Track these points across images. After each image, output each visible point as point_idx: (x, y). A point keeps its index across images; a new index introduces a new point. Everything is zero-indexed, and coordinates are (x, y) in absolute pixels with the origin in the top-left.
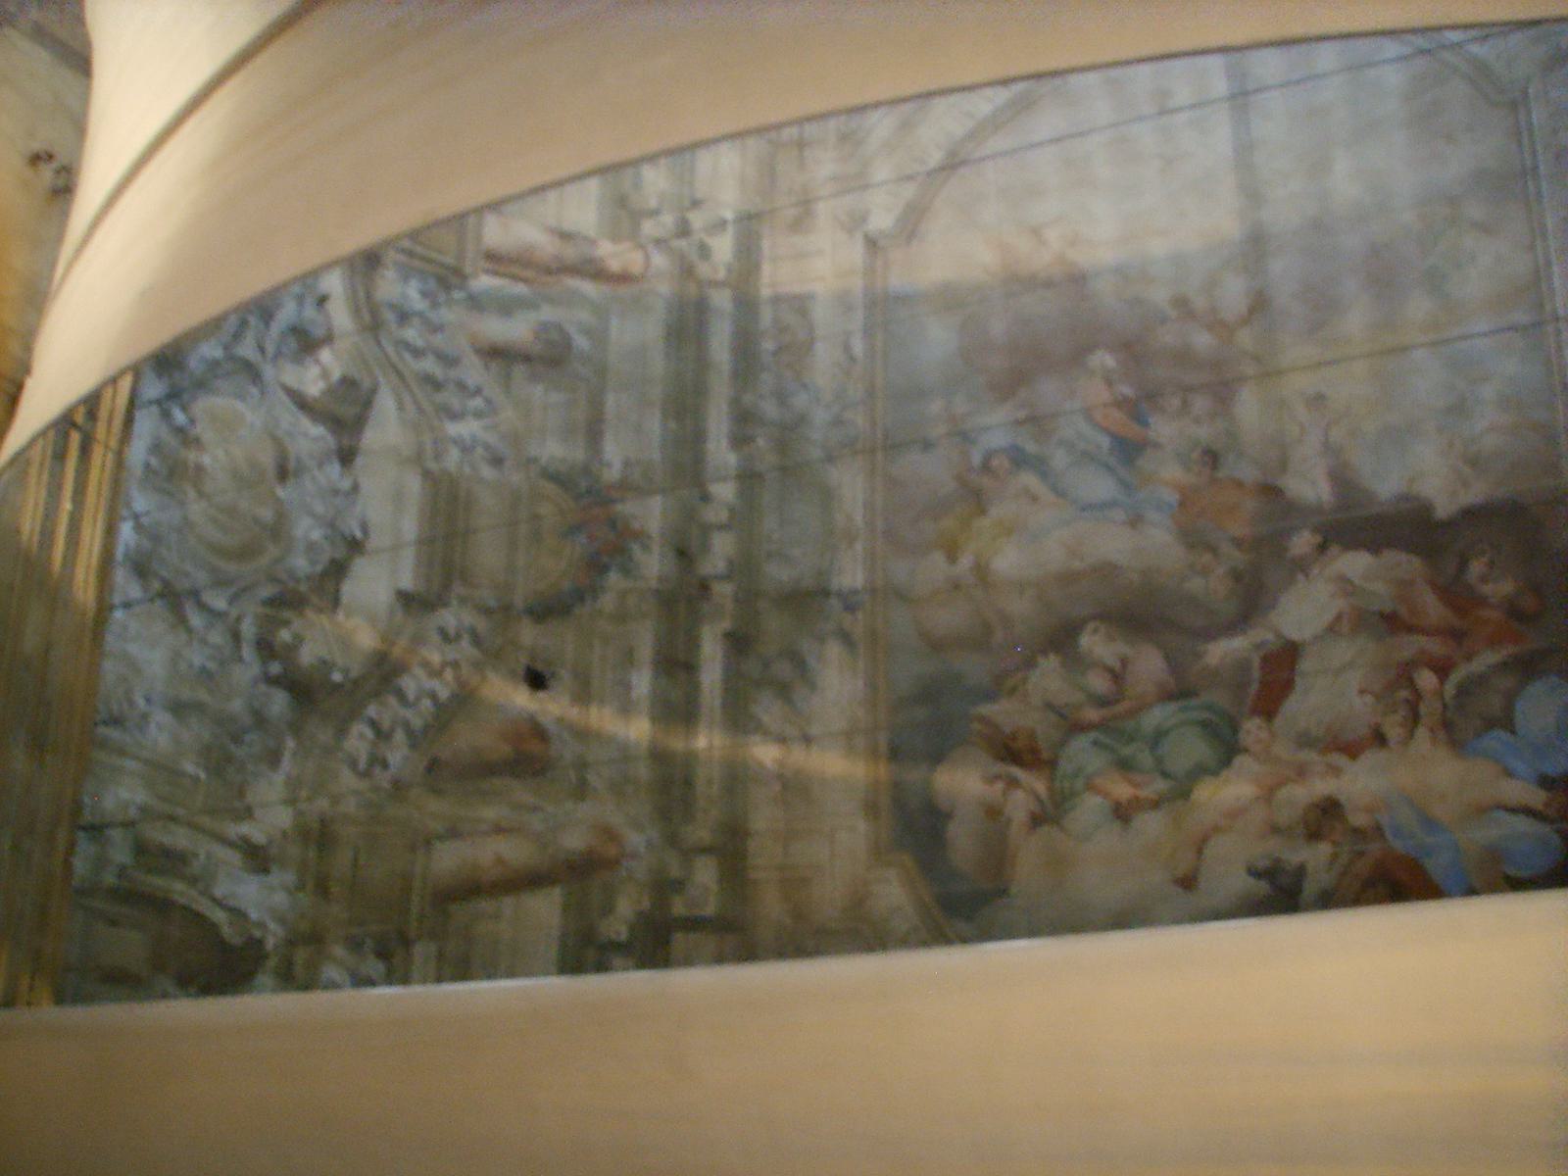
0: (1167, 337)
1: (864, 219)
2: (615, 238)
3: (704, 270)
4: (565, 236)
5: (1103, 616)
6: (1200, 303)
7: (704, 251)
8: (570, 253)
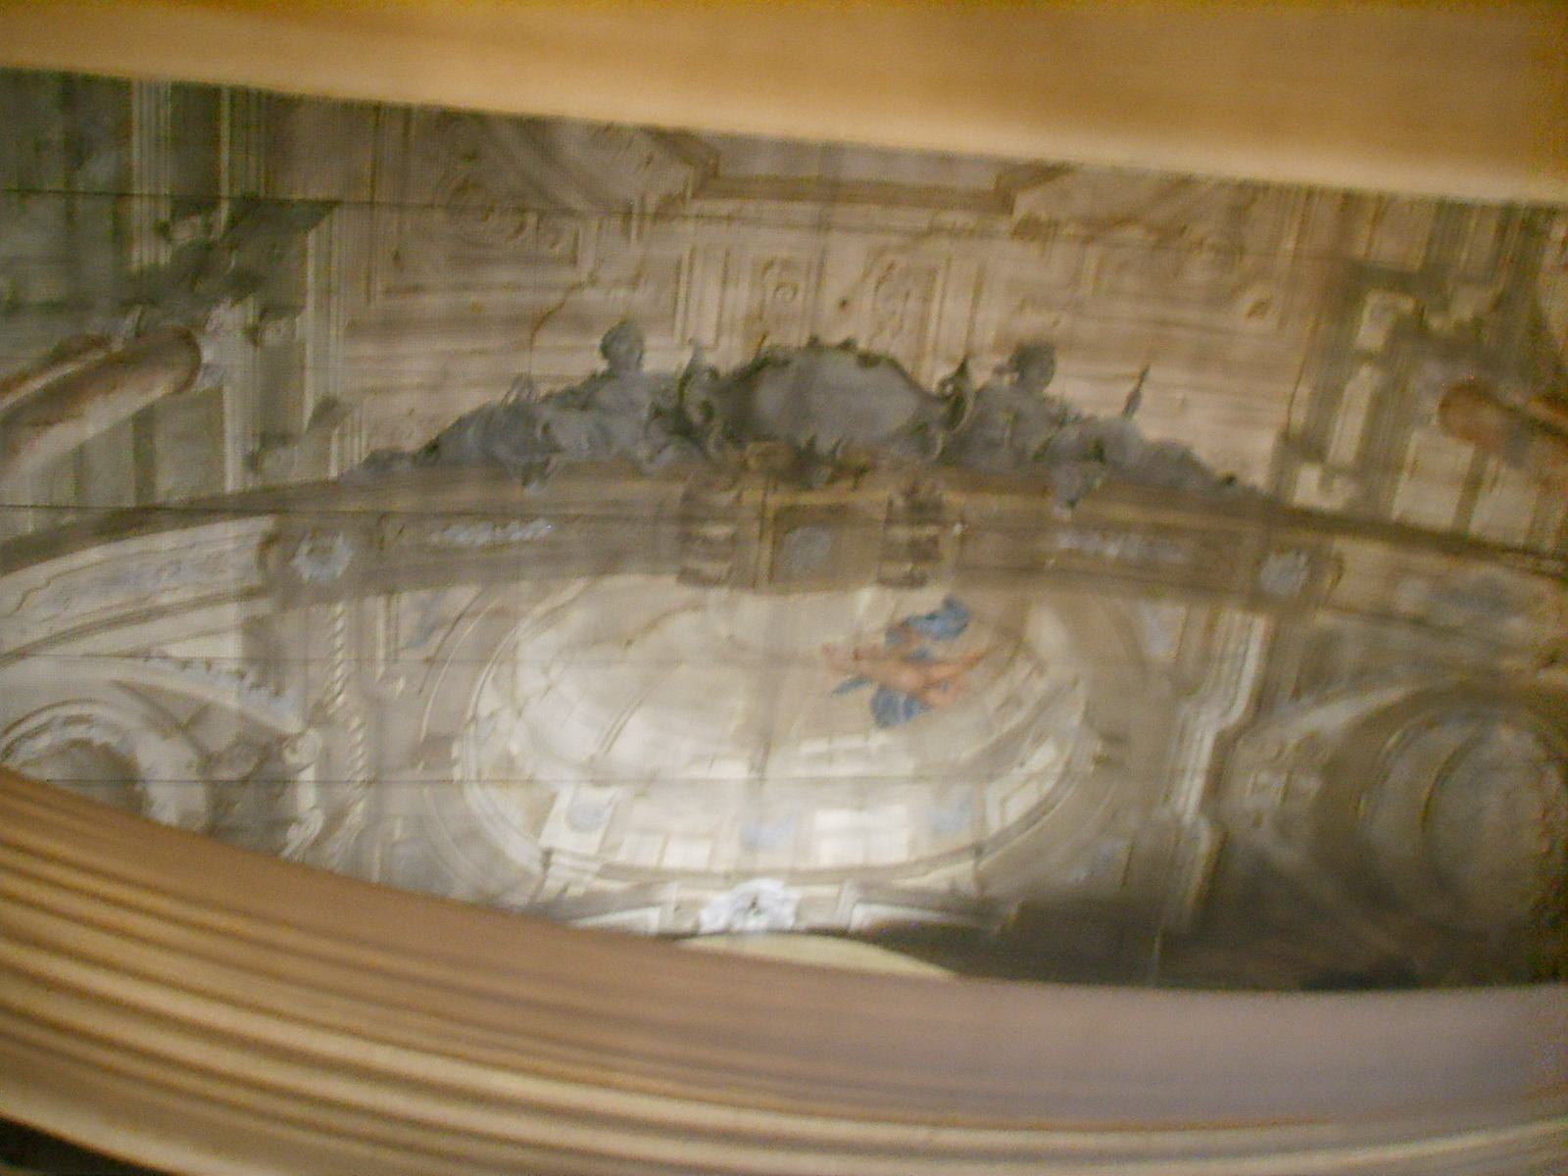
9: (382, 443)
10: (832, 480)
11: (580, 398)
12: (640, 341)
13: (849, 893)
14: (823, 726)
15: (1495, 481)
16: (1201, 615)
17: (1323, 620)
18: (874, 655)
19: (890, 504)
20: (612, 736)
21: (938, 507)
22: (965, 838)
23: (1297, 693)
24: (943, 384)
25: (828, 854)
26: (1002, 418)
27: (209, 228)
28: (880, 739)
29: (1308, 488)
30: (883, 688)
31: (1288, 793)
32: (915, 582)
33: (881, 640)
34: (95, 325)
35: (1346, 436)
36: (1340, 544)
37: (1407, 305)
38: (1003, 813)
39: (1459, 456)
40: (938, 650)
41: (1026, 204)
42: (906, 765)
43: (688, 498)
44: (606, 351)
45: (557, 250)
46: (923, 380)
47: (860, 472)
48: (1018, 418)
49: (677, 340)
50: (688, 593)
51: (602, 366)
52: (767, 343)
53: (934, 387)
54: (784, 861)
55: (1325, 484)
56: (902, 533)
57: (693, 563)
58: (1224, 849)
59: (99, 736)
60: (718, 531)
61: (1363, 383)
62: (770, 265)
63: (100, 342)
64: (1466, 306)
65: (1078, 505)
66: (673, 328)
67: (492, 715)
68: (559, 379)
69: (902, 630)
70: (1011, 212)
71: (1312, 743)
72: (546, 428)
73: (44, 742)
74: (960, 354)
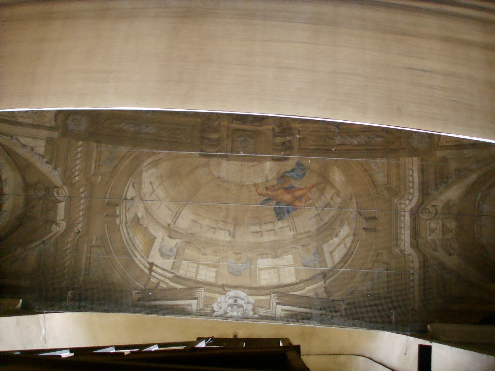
13: (274, 299)
14: (258, 221)
16: (393, 161)
17: (439, 154)
18: (273, 188)
19: (273, 129)
20: (177, 216)
22: (318, 269)
23: (437, 188)
28: (280, 224)
31: (445, 230)
33: (275, 182)
38: (332, 257)
40: (297, 184)
42: (289, 234)
50: (204, 160)
56: (279, 140)
58: (425, 265)
60: (214, 136)
65: (340, 127)
67: (132, 199)
69: (282, 177)
71: (447, 205)
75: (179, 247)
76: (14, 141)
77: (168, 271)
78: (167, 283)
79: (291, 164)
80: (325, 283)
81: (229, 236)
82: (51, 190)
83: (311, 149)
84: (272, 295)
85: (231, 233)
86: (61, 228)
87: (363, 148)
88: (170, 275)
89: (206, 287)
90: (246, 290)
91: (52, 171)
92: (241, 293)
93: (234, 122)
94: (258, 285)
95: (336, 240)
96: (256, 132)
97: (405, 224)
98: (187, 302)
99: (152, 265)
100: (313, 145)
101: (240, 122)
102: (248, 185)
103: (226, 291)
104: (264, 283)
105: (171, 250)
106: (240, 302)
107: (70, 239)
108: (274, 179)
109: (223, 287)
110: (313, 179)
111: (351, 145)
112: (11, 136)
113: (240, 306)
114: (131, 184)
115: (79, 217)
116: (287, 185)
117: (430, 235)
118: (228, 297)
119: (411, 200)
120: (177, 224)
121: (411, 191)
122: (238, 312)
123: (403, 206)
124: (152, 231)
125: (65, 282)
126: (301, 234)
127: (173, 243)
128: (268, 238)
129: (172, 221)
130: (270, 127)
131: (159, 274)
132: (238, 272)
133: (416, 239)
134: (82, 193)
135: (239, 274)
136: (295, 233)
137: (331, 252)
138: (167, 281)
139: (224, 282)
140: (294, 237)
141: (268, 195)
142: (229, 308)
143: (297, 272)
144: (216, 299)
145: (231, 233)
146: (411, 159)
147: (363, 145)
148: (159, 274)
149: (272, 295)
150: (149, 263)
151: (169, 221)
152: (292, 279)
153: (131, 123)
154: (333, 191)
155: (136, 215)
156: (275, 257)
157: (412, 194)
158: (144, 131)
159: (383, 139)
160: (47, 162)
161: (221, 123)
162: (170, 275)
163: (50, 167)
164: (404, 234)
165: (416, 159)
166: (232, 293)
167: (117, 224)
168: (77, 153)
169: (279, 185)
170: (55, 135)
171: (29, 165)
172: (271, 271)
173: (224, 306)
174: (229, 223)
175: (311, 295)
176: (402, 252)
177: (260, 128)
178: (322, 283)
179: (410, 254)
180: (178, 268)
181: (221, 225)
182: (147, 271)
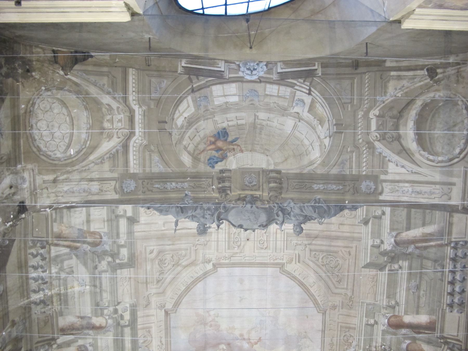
0: (238, 343)
1: (164, 306)
2: (97, 316)
3: (122, 322)
4: (82, 318)
5: (417, 8)
6: (246, 337)
7: (122, 317)
8: (84, 322)
9: (354, 212)
10: (246, 197)
11: (307, 219)
12: (294, 231)
13: (227, 75)
15: (83, 224)
21: (219, 192)
24: (223, 223)
25: (232, 88)
26: (208, 216)
27: (391, 266)
28: (225, 125)
29: (129, 209)
30: (226, 140)
31: (111, 121)
32: (222, 171)
33: (228, 154)
34: (417, 252)
35: (123, 223)
36: (117, 197)
37: (118, 261)
38: (188, 103)
39: (94, 227)
40: (214, 153)
41: (209, 267)
43: (281, 193)
44: (302, 229)
45: (314, 253)
46: (227, 222)
47: (239, 199)
48: (203, 217)
49: (286, 231)
50: (278, 168)
51: (302, 225)
52: (265, 231)
53: (224, 221)
54: (245, 85)
55: (125, 211)
56: (227, 184)
57: (278, 176)
59: (425, 154)
60: (272, 185)
61: (123, 240)
62: (266, 248)
63: (417, 248)
64: (103, 265)
65: (184, 195)
66: (287, 233)
67: (326, 137)
68: (312, 223)
69: (223, 158)
70: (213, 264)
71: (110, 137)
72: (315, 212)
73: (440, 158)
74: (219, 230)
75: (292, 107)
76: (410, 170)
77: (298, 90)
78: (298, 82)
79: (219, 166)
80: (192, 86)
81: (258, 116)
82: (381, 138)
83: (204, 178)
84: (227, 77)
85: (257, 117)
86: (373, 113)
87: (168, 180)
88: (296, 87)
89: (272, 81)
90: (245, 80)
91: (382, 151)
92: (248, 78)
93: (259, 196)
94: (237, 84)
95: (186, 115)
96: (244, 190)
97: (139, 126)
98: (284, 70)
99: (309, 94)
100: (203, 181)
101: (255, 196)
102: (248, 151)
103: (258, 79)
104: (234, 85)
105: (297, 104)
106: (249, 72)
107: (366, 106)
108: (230, 156)
109: (261, 82)
110: (202, 157)
111: (177, 183)
112: (412, 172)
113: (249, 69)
114: (327, 147)
115: (361, 122)
116: (221, 152)
117: (122, 117)
118: (257, 74)
119: (135, 142)
120: (294, 122)
121: (135, 144)
122: (250, 65)
123: (140, 138)
124: (311, 117)
125: (367, 77)
126: (210, 118)
127: (297, 109)
128: (231, 115)
129: (297, 124)
130: (233, 193)
131: (305, 88)
132: (251, 92)
133: (132, 116)
134: (360, 139)
135: (250, 91)
136: (214, 119)
137: (189, 106)
138: (298, 84)
139: (259, 85)
140: (214, 116)
141: (233, 145)
142: (255, 68)
143: (211, 92)
144: (265, 73)
145: (257, 117)
146: (135, 172)
147: (168, 182)
148: (305, 88)
149: (227, 77)
150: (311, 95)
151: (299, 124)
152: (214, 88)
153: (330, 190)
154: (188, 149)
155: (322, 127)
156: (227, 103)
157: (134, 147)
158: (321, 185)
159: (154, 186)
160: (386, 157)
161: (267, 195)
162: (296, 87)
163: (383, 154)
164: (139, 119)
165: (132, 172)
166: (254, 78)
167: (334, 120)
168: (366, 166)
169: (226, 152)
170: (383, 177)
171: (399, 154)
172: (229, 93)
173: (260, 69)
174: (259, 125)
175: (201, 78)
176: (140, 107)
177: (239, 192)
178: (194, 86)
179: (135, 105)
180: (291, 93)
181: (264, 123)
182: (312, 89)
